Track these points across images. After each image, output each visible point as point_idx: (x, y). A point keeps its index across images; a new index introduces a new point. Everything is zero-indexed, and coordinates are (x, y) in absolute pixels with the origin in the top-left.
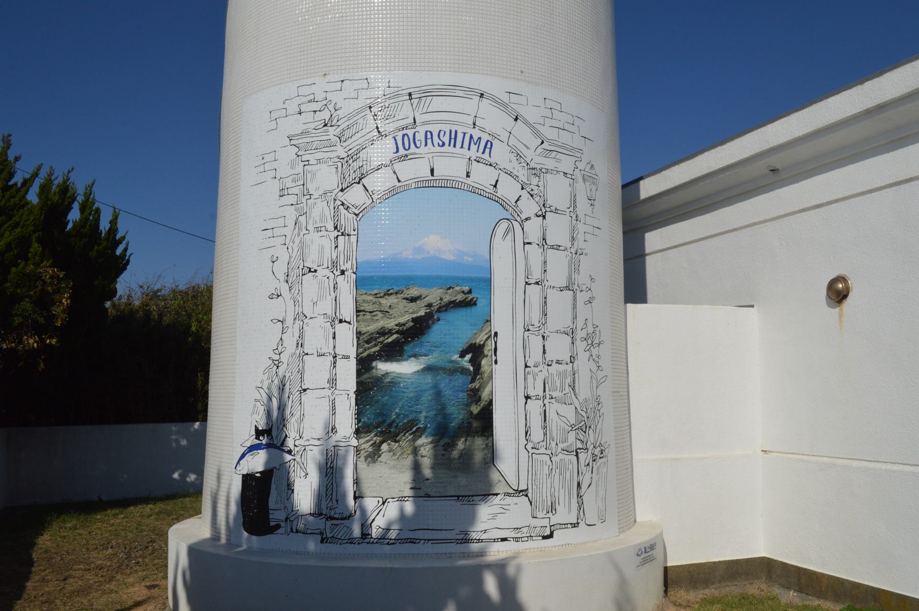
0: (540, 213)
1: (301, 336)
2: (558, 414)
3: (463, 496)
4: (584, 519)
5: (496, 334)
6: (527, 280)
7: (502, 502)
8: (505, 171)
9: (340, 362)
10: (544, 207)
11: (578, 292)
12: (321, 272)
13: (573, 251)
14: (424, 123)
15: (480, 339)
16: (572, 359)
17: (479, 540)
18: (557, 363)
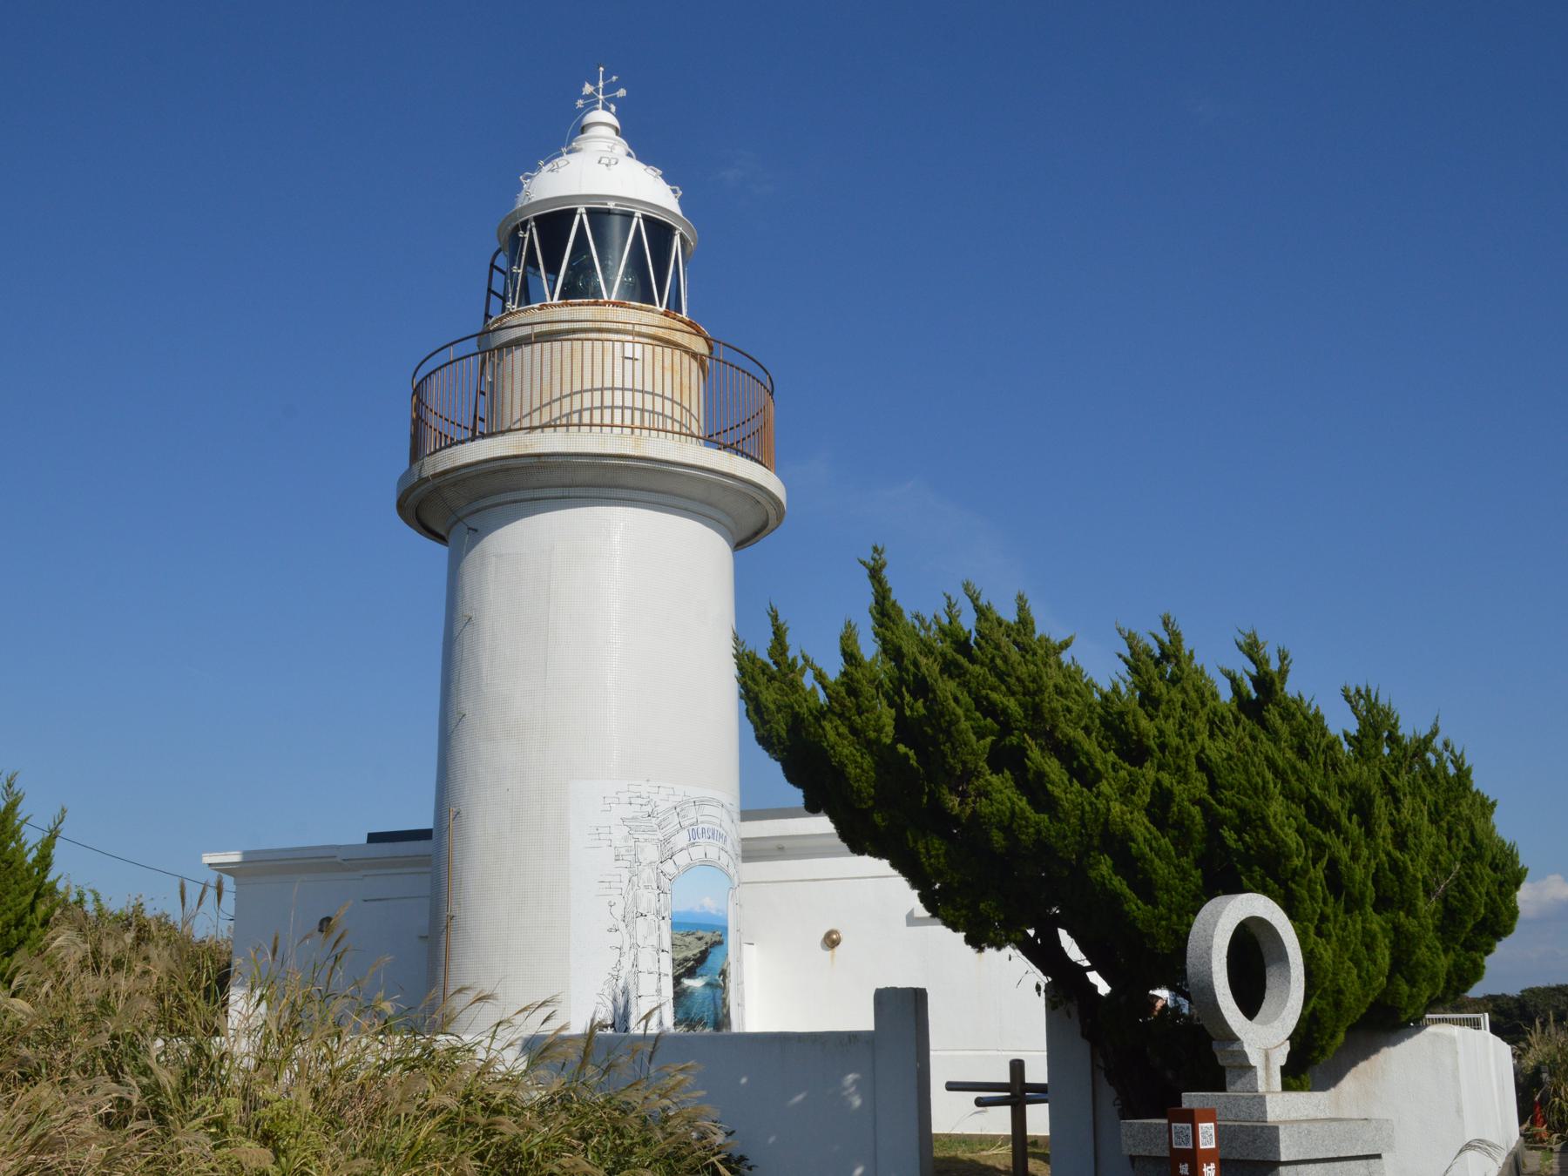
1: (636, 959)
9: (663, 978)
12: (650, 917)
14: (702, 822)
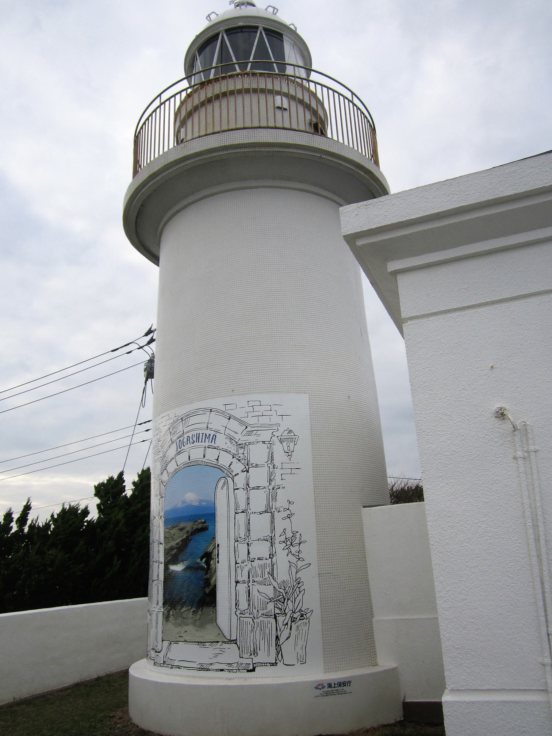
0: (245, 469)
2: (259, 592)
3: (201, 642)
4: (282, 660)
5: (218, 545)
6: (236, 511)
7: (221, 647)
8: (222, 450)
10: (248, 466)
11: (276, 513)
13: (271, 487)
14: (188, 432)
15: (210, 549)
16: (271, 556)
17: (208, 669)
18: (259, 559)
